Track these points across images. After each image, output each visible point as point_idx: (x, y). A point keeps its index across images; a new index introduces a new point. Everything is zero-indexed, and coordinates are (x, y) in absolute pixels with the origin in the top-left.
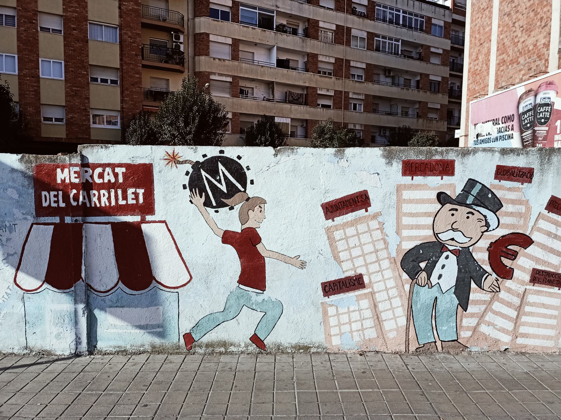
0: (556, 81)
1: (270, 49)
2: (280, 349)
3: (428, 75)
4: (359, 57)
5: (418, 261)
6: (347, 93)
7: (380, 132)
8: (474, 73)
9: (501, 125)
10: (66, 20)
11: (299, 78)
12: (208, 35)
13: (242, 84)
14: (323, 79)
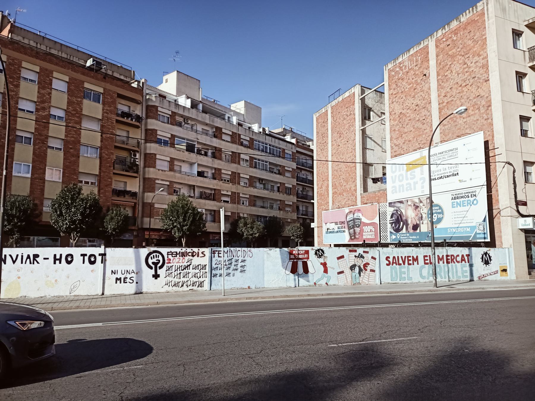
0: (361, 210)
1: (192, 164)
2: (331, 285)
3: (284, 184)
4: (246, 172)
5: (352, 268)
6: (239, 193)
7: (258, 219)
8: (320, 195)
9: (339, 225)
10: (66, 142)
11: (209, 183)
12: (155, 155)
13: (176, 186)
14: (224, 184)
